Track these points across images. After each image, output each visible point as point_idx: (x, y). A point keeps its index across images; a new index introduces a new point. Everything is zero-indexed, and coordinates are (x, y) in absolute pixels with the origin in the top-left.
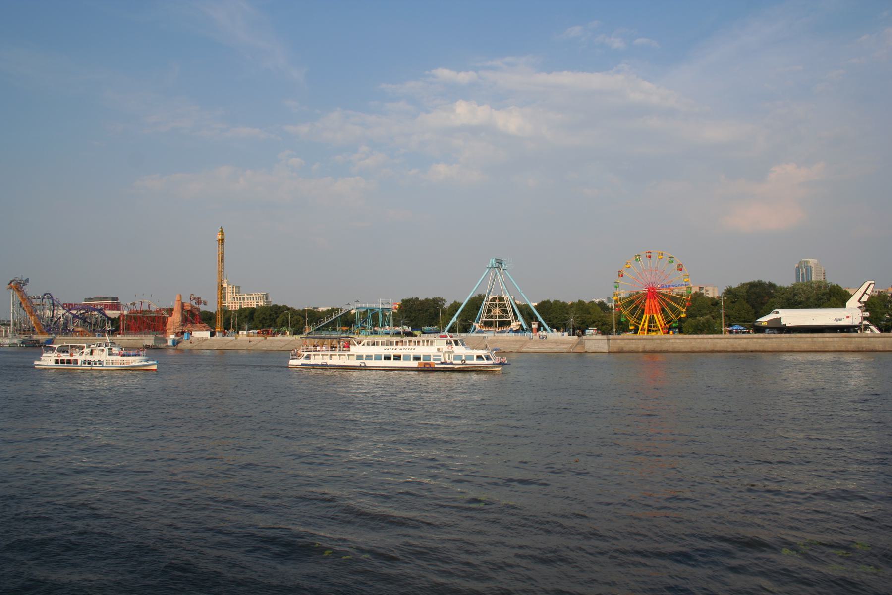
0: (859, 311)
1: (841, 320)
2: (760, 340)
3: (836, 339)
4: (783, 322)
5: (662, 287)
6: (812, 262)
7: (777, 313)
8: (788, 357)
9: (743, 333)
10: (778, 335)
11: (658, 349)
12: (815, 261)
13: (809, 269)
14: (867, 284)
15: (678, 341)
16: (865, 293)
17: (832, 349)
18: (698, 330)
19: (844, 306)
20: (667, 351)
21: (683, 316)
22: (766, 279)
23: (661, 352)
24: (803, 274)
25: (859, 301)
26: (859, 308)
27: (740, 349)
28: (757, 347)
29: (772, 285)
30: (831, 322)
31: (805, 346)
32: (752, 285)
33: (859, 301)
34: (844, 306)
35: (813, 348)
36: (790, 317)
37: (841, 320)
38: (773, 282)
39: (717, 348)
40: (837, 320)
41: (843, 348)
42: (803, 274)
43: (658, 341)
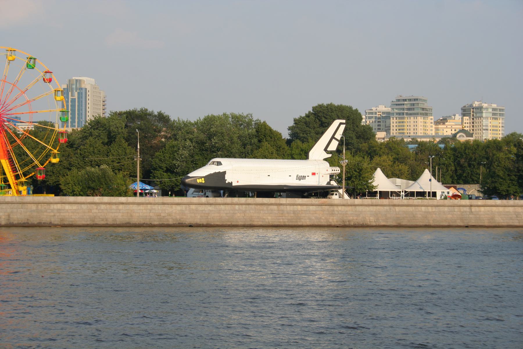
0: (327, 164)
1: (304, 177)
2: (201, 208)
3: (311, 208)
4: (228, 179)
5: (409, 107)
6: (88, 82)
7: (219, 164)
8: (233, 237)
9: (151, 194)
10: (211, 200)
11: (36, 222)
12: (92, 81)
13: (82, 93)
14: (337, 122)
15: (67, 207)
16: (333, 137)
17: (308, 223)
18: (91, 187)
19: (306, 157)
20: (50, 225)
21: (55, 161)
22: (154, 107)
23: (40, 225)
24: (73, 101)
25: (326, 150)
26: (325, 160)
27: (171, 222)
28: (198, 220)
29: (163, 118)
30: (293, 182)
31: (270, 219)
32: (131, 116)
33: (326, 150)
34: (306, 157)
35: (281, 222)
36: (239, 171)
37: (304, 177)
38: (166, 112)
39: (135, 220)
40: (300, 178)
41: (324, 223)
42: (73, 101)
43: (34, 207)
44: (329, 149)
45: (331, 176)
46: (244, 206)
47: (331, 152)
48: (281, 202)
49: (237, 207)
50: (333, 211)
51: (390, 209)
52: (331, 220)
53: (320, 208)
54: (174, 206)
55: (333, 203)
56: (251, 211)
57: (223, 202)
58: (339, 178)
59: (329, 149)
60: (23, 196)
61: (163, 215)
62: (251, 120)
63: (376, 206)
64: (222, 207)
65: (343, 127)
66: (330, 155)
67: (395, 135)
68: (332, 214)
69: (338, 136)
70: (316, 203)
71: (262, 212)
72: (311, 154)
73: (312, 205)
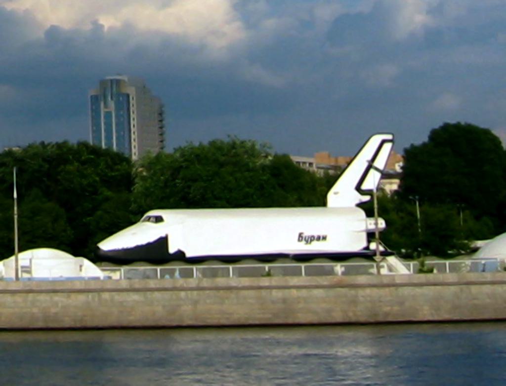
0: (362, 213)
7: (159, 219)
16: (370, 167)
25: (358, 188)
26: (361, 205)
33: (358, 188)
41: (338, 317)
44: (364, 187)
45: (371, 236)
46: (195, 293)
47: (368, 192)
48: (262, 284)
49: (183, 294)
50: (356, 296)
51: (462, 290)
52: (351, 314)
53: (332, 292)
54: (73, 296)
55: (357, 283)
56: (208, 301)
57: (158, 286)
58: (383, 237)
59: (364, 187)
60: (435, 274)
61: (53, 310)
62: (234, 143)
63: (435, 284)
64: (157, 295)
65: (387, 147)
66: (367, 198)
67: (319, 189)
68: (354, 302)
69: (380, 163)
70: (325, 283)
71: (227, 301)
72: (331, 196)
73: (317, 287)
